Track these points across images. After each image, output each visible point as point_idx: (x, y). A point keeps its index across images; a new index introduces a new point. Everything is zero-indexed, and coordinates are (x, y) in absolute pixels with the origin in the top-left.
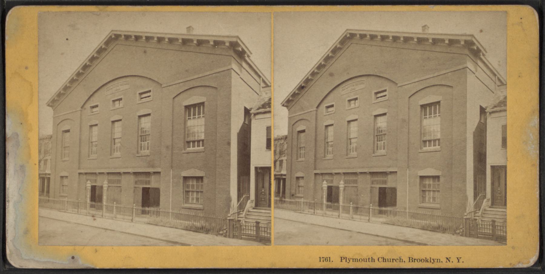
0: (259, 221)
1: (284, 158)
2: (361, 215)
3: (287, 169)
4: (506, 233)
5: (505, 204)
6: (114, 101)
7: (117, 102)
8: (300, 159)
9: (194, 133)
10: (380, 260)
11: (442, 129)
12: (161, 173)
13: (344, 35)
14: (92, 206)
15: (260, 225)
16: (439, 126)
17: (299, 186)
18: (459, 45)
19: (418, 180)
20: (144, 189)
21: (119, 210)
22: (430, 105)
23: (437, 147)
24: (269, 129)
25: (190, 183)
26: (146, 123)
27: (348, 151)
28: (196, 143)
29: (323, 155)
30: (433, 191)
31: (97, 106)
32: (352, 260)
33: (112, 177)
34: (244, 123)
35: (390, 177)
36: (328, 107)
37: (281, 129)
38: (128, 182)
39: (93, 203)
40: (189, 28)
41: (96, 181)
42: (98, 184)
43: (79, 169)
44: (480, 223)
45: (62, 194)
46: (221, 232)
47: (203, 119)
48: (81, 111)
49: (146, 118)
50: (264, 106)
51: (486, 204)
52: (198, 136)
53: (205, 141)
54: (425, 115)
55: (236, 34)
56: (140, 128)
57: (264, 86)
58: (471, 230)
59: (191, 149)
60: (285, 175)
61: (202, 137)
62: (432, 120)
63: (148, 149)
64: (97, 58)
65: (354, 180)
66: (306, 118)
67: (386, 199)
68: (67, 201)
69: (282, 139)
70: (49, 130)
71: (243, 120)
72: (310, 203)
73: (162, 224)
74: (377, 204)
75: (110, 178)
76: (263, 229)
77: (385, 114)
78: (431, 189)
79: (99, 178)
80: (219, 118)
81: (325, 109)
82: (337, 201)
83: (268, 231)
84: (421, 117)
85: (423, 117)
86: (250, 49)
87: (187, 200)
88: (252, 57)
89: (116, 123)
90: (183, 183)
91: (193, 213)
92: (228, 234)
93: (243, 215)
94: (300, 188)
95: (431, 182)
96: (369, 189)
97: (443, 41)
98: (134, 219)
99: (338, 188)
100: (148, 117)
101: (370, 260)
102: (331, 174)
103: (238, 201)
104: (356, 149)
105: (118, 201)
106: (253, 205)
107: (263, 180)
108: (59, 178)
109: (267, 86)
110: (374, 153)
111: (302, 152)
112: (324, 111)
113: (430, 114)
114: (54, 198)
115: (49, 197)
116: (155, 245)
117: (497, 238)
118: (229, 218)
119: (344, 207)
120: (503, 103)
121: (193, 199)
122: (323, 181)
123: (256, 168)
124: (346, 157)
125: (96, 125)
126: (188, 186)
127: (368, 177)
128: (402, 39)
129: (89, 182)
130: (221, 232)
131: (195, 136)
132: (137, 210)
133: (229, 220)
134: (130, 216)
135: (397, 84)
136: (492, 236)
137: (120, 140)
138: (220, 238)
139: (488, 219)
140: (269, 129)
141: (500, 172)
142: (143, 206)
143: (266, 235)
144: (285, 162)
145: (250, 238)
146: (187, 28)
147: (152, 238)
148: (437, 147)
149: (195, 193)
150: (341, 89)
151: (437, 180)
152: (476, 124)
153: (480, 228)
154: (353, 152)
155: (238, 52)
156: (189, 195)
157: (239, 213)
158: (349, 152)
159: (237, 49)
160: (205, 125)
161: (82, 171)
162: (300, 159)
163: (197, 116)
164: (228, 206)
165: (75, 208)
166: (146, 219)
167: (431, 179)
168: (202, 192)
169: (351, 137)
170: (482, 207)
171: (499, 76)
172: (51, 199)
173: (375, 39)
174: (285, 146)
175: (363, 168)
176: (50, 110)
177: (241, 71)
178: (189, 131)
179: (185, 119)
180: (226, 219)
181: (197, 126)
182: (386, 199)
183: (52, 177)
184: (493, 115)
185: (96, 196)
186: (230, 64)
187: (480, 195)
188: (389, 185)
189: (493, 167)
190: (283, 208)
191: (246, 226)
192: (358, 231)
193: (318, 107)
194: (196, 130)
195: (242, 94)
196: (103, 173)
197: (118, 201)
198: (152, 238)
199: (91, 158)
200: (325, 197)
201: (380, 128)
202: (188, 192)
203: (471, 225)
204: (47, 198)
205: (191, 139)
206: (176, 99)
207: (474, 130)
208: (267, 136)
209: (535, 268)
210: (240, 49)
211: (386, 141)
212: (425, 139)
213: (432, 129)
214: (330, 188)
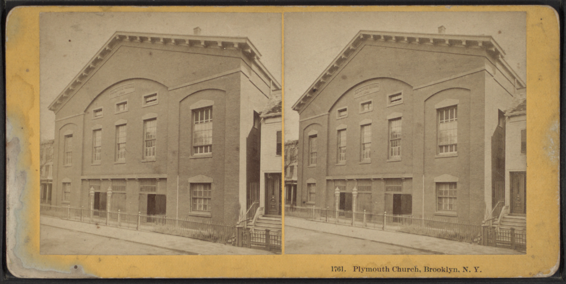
0: (515, 228)
1: (295, 164)
2: (129, 223)
4: (526, 241)
5: (525, 212)
6: (118, 105)
8: (311, 165)
9: (201, 138)
10: (395, 269)
11: (459, 134)
14: (95, 214)
15: (270, 233)
18: (477, 47)
19: (434, 186)
20: (149, 196)
22: (447, 109)
23: (454, 153)
24: (279, 134)
26: (152, 128)
27: (361, 156)
28: (199, 148)
29: (335, 161)
30: (450, 198)
32: (365, 270)
34: (254, 127)
35: (405, 184)
36: (341, 111)
37: (292, 133)
38: (133, 189)
39: (97, 210)
40: (196, 29)
41: (99, 187)
42: (102, 191)
43: (82, 175)
44: (499, 231)
45: (65, 201)
46: (230, 241)
47: (211, 124)
48: (84, 115)
49: (152, 122)
50: (274, 110)
51: (504, 211)
52: (206, 141)
53: (458, 146)
55: (245, 36)
57: (274, 89)
58: (489, 238)
59: (199, 154)
60: (296, 182)
66: (318, 122)
67: (401, 206)
68: (70, 209)
69: (292, 144)
70: (51, 135)
73: (168, 232)
75: (114, 185)
79: (103, 185)
80: (227, 123)
81: (337, 113)
82: (350, 208)
83: (279, 240)
85: (440, 121)
86: (260, 51)
87: (194, 208)
88: (262, 59)
89: (121, 128)
91: (200, 221)
92: (236, 242)
93: (252, 223)
94: (312, 195)
95: (448, 189)
96: (383, 196)
97: (460, 42)
98: (139, 227)
99: (351, 195)
100: (154, 121)
101: (385, 269)
104: (370, 154)
105: (122, 209)
106: (263, 212)
107: (273, 186)
108: (62, 185)
109: (278, 89)
110: (388, 158)
111: (314, 157)
112: (337, 115)
113: (447, 118)
114: (56, 205)
117: (516, 247)
118: (237, 226)
120: (523, 106)
121: (200, 206)
122: (336, 187)
123: (266, 174)
125: (100, 130)
126: (195, 193)
127: (383, 183)
128: (417, 40)
129: (92, 189)
130: (230, 241)
131: (202, 141)
132: (142, 217)
133: (238, 228)
134: (135, 224)
135: (412, 87)
136: (511, 244)
137: (124, 145)
138: (228, 247)
139: (507, 227)
140: (279, 134)
141: (519, 178)
142: (149, 213)
144: (296, 167)
145: (259, 247)
146: (194, 29)
147: (157, 247)
148: (454, 153)
149: (203, 200)
150: (354, 93)
151: (453, 186)
152: (494, 129)
154: (367, 157)
156: (196, 202)
157: (248, 221)
158: (362, 157)
159: (246, 50)
160: (213, 130)
162: (311, 165)
164: (237, 214)
165: (78, 216)
166: (151, 227)
168: (209, 199)
170: (501, 215)
171: (518, 79)
172: (52, 206)
174: (52, 151)
176: (52, 114)
177: (250, 74)
178: (196, 135)
179: (192, 123)
180: (235, 227)
181: (205, 130)
182: (401, 206)
183: (54, 184)
185: (99, 203)
186: (239, 66)
187: (499, 202)
189: (512, 173)
191: (255, 234)
192: (371, 239)
193: (330, 111)
194: (203, 135)
195: (251, 98)
196: (107, 179)
197: (122, 209)
198: (157, 247)
199: (94, 164)
200: (92, 203)
201: (394, 132)
202: (195, 199)
203: (489, 233)
204: (49, 205)
205: (199, 144)
206: (183, 103)
207: (492, 135)
208: (277, 140)
209: (556, 278)
211: (400, 146)
214: (342, 195)
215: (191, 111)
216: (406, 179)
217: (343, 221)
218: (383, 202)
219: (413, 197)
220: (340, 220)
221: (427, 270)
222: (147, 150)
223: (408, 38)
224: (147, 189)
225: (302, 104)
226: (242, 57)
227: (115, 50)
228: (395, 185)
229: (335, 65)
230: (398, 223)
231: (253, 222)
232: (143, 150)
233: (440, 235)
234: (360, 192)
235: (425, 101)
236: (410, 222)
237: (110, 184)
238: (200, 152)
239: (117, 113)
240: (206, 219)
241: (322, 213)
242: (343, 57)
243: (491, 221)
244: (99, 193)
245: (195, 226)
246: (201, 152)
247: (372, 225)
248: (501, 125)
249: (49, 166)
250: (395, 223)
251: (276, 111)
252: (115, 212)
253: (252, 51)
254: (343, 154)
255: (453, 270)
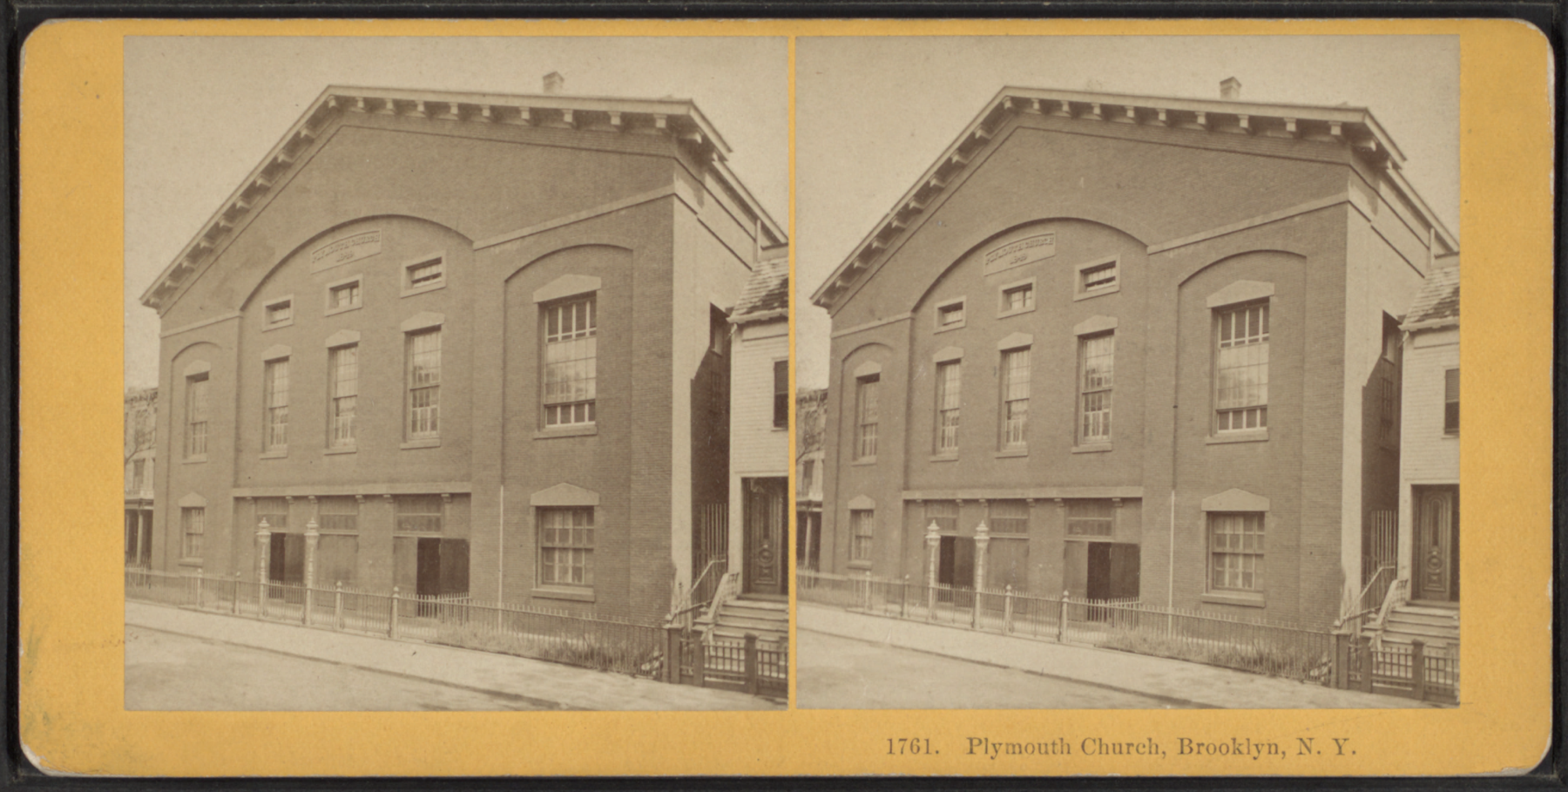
0: (755, 633)
1: (818, 456)
2: (368, 618)
3: (154, 485)
4: (786, 672)
5: (1455, 596)
6: (1009, 292)
7: (344, 294)
8: (193, 458)
9: (566, 380)
10: (1090, 746)
11: (599, 371)
12: (1144, 502)
13: (996, 102)
14: (273, 593)
15: (1426, 652)
16: (593, 364)
17: (859, 537)
18: (1326, 139)
19: (1202, 522)
20: (424, 545)
21: (352, 604)
22: (565, 303)
23: (1259, 430)
24: (781, 368)
25: (557, 523)
26: (428, 353)
28: (1245, 415)
30: (1245, 555)
31: (286, 305)
32: (1265, 750)
33: (329, 510)
34: (1383, 359)
35: (1120, 514)
36: (946, 310)
37: (813, 372)
38: (377, 523)
39: (278, 584)
41: (284, 521)
42: (291, 529)
43: (907, 487)
44: (1380, 648)
46: (646, 667)
47: (593, 341)
48: (241, 318)
51: (1395, 594)
52: (578, 390)
54: (564, 330)
55: (685, 96)
56: (411, 368)
57: (1441, 251)
58: (1353, 668)
59: (558, 427)
60: (819, 505)
61: (591, 392)
62: (1245, 350)
63: (434, 427)
64: (960, 167)
65: (1100, 525)
66: (879, 339)
67: (1108, 577)
68: (203, 580)
69: (811, 399)
70: (146, 375)
71: (1379, 351)
72: (889, 585)
73: (476, 643)
74: (1084, 590)
75: (995, 516)
76: (1433, 663)
77: (1109, 333)
78: (1240, 549)
80: (636, 339)
82: (969, 581)
83: (782, 663)
84: (1213, 344)
87: (547, 576)
88: (733, 161)
90: (537, 527)
91: (1232, 617)
92: (665, 670)
93: (1377, 624)
94: (864, 543)
95: (1240, 531)
96: (1061, 549)
97: (1279, 123)
98: (395, 629)
99: (971, 543)
100: (434, 335)
101: (1058, 748)
102: (952, 502)
103: (1364, 581)
104: (353, 428)
105: (1020, 583)
107: (1436, 524)
108: (179, 513)
109: (1449, 252)
110: (1076, 443)
112: (935, 323)
113: (1240, 334)
114: (165, 569)
115: (150, 568)
116: (1130, 706)
117: (1426, 693)
118: (668, 626)
119: (317, 593)
120: (1450, 305)
121: (564, 571)
122: (929, 522)
123: (745, 481)
124: (997, 454)
125: (957, 361)
127: (1061, 512)
128: (1162, 117)
129: (264, 523)
130: (646, 667)
132: (403, 603)
133: (669, 630)
134: (1053, 624)
135: (471, 242)
136: (747, 680)
137: (351, 403)
138: (1310, 690)
140: (781, 368)
141: (1439, 500)
142: (422, 589)
143: (774, 675)
144: (149, 465)
145: (728, 683)
146: (1223, 83)
147: (446, 684)
148: (1259, 430)
149: (571, 555)
150: (985, 259)
152: (1371, 367)
153: (1378, 663)
154: (1016, 439)
155: (689, 145)
156: (1223, 566)
157: (696, 612)
158: (1004, 439)
159: (1365, 144)
160: (598, 358)
161: (246, 492)
162: (193, 458)
163: (1247, 338)
166: (431, 628)
167: (1241, 522)
169: (340, 393)
171: (1440, 231)
172: (156, 572)
173: (1085, 116)
174: (822, 421)
175: (1042, 486)
176: (822, 317)
177: (701, 203)
178: (551, 373)
179: (540, 339)
180: (660, 629)
181: (576, 360)
182: (1108, 577)
183: (827, 514)
184: (1421, 341)
185: (284, 564)
186: (669, 181)
188: (1119, 537)
189: (1418, 490)
190: (145, 597)
191: (716, 648)
192: (1027, 668)
193: (916, 309)
195: (705, 269)
196: (976, 501)
197: (1020, 583)
198: (446, 684)
200: (263, 564)
201: (1094, 371)
202: (548, 551)
203: (1353, 655)
205: (557, 398)
206: (516, 282)
207: (1365, 382)
208: (777, 388)
209: (1539, 776)
210: (1373, 146)
212: (551, 400)
213: (1244, 378)
214: (947, 544)
215: (1209, 313)
216: (1125, 501)
217: (278, 611)
218: (1061, 565)
219: (472, 547)
220: (942, 614)
221: (1186, 750)
222: (1087, 418)
223: (461, 107)
224: (1086, 528)
225: (169, 288)
226: (677, 153)
227: (1001, 138)
228: (1094, 517)
229: (933, 182)
230: (1102, 624)
231: (1379, 621)
232: (1076, 420)
233: (547, 652)
234: (324, 532)
235: (1181, 286)
236: (1134, 619)
237: (314, 509)
238: (577, 420)
239: (334, 311)
240: (579, 606)
241: (888, 592)
242: (956, 158)
243: (1359, 621)
244: (283, 535)
245: (550, 625)
246: (1237, 425)
247: (1029, 627)
248: (717, 349)
249: (813, 462)
250: (420, 619)
251: (774, 305)
252: (327, 588)
253: (1379, 145)
254: (279, 427)
255: (1266, 748)
